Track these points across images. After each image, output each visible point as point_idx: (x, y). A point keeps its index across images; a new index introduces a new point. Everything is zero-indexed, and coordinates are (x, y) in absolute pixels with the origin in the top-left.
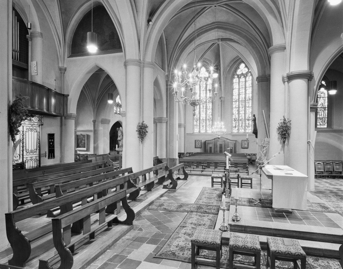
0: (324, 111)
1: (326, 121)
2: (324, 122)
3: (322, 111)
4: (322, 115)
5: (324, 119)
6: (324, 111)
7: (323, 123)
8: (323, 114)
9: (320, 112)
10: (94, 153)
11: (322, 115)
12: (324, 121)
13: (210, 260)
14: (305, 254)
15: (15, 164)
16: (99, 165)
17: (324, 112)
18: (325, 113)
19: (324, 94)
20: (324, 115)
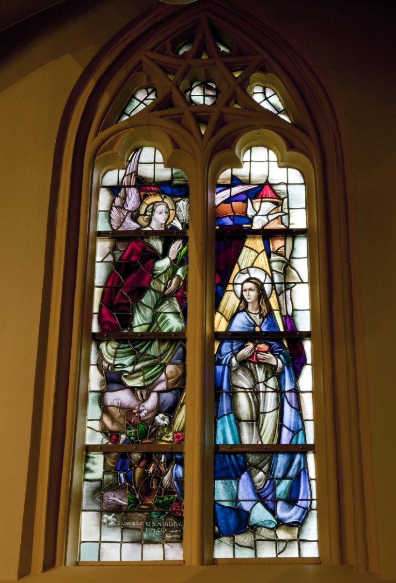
0: (279, 376)
1: (310, 489)
2: (291, 500)
3: (261, 374)
4: (269, 422)
5: (281, 460)
6: (279, 376)
7: (282, 512)
8: (270, 401)
9: (243, 381)
10: (250, 441)
11: (269, 422)
12: (283, 487)
13: (182, 401)
14: (133, 357)
15: (75, 483)
16: (136, 467)
17: (288, 386)
18: (296, 391)
19: (279, 200)
20: (289, 414)
